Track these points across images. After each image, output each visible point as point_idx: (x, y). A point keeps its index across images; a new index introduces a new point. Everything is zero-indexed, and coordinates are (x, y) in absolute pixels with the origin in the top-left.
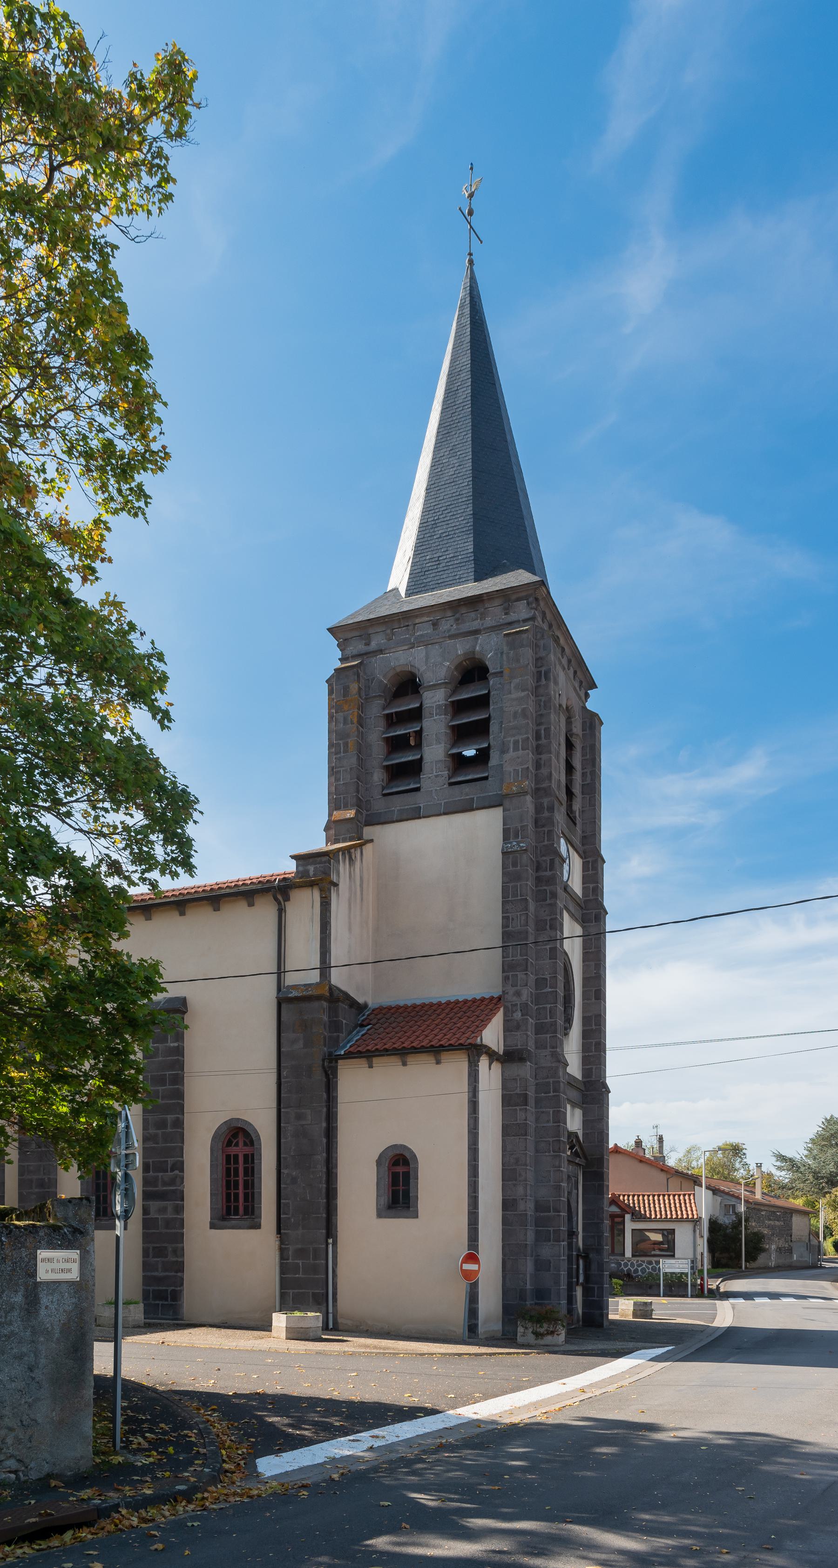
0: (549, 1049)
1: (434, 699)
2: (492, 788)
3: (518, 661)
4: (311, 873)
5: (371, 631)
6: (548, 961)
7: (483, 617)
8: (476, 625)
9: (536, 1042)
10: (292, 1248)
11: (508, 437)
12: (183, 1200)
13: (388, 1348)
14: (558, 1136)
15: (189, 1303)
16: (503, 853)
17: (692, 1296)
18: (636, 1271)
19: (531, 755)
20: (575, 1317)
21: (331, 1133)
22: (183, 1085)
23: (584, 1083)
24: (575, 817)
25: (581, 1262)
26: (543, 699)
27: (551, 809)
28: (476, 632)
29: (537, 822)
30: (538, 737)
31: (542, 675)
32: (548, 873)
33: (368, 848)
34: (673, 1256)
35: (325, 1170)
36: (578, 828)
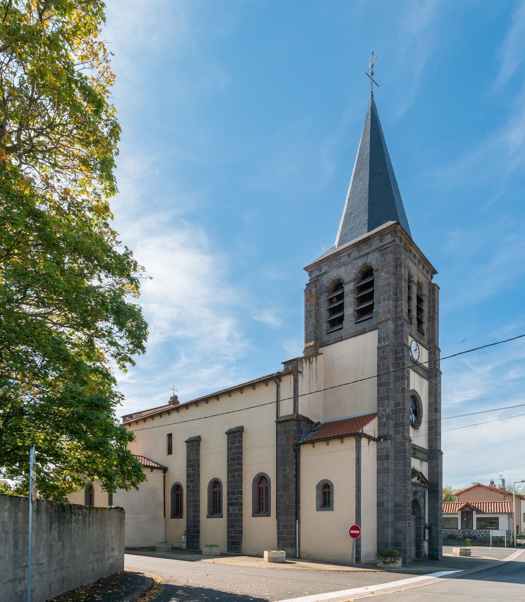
0: (401, 434)
1: (349, 288)
2: (374, 321)
3: (385, 261)
4: (290, 369)
5: (322, 265)
6: (400, 394)
7: (371, 246)
8: (367, 251)
9: (395, 432)
10: (281, 524)
11: (389, 167)
12: (242, 505)
13: (310, 567)
14: (405, 473)
15: (245, 545)
16: (378, 348)
17: (507, 547)
18: (479, 535)
19: (392, 302)
20: (423, 555)
21: (297, 476)
22: (242, 460)
23: (429, 450)
24: (424, 332)
25: (427, 531)
26: (399, 276)
27: (402, 325)
28: (368, 254)
29: (395, 333)
30: (396, 294)
31: (398, 265)
32: (401, 354)
33: (320, 358)
34: (498, 529)
35: (295, 491)
36: (426, 337)
